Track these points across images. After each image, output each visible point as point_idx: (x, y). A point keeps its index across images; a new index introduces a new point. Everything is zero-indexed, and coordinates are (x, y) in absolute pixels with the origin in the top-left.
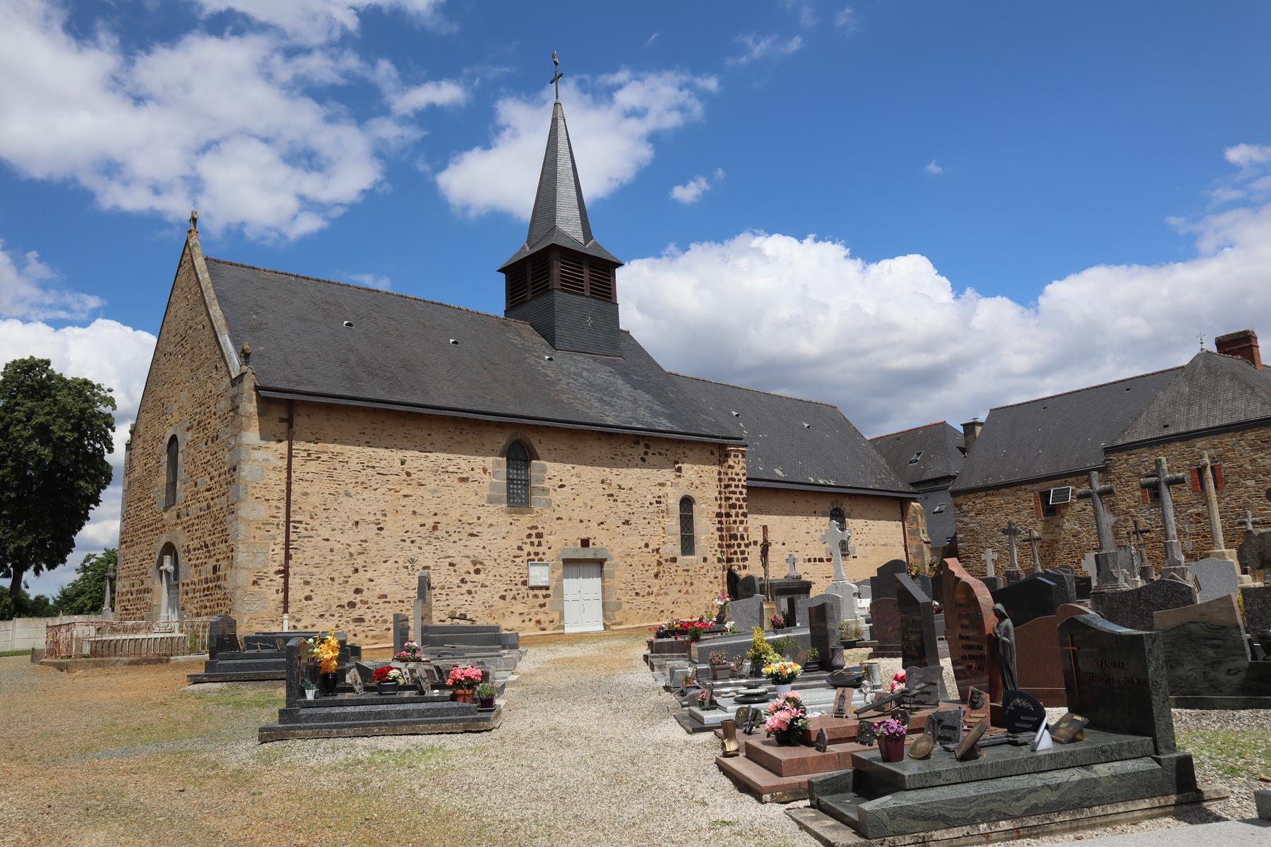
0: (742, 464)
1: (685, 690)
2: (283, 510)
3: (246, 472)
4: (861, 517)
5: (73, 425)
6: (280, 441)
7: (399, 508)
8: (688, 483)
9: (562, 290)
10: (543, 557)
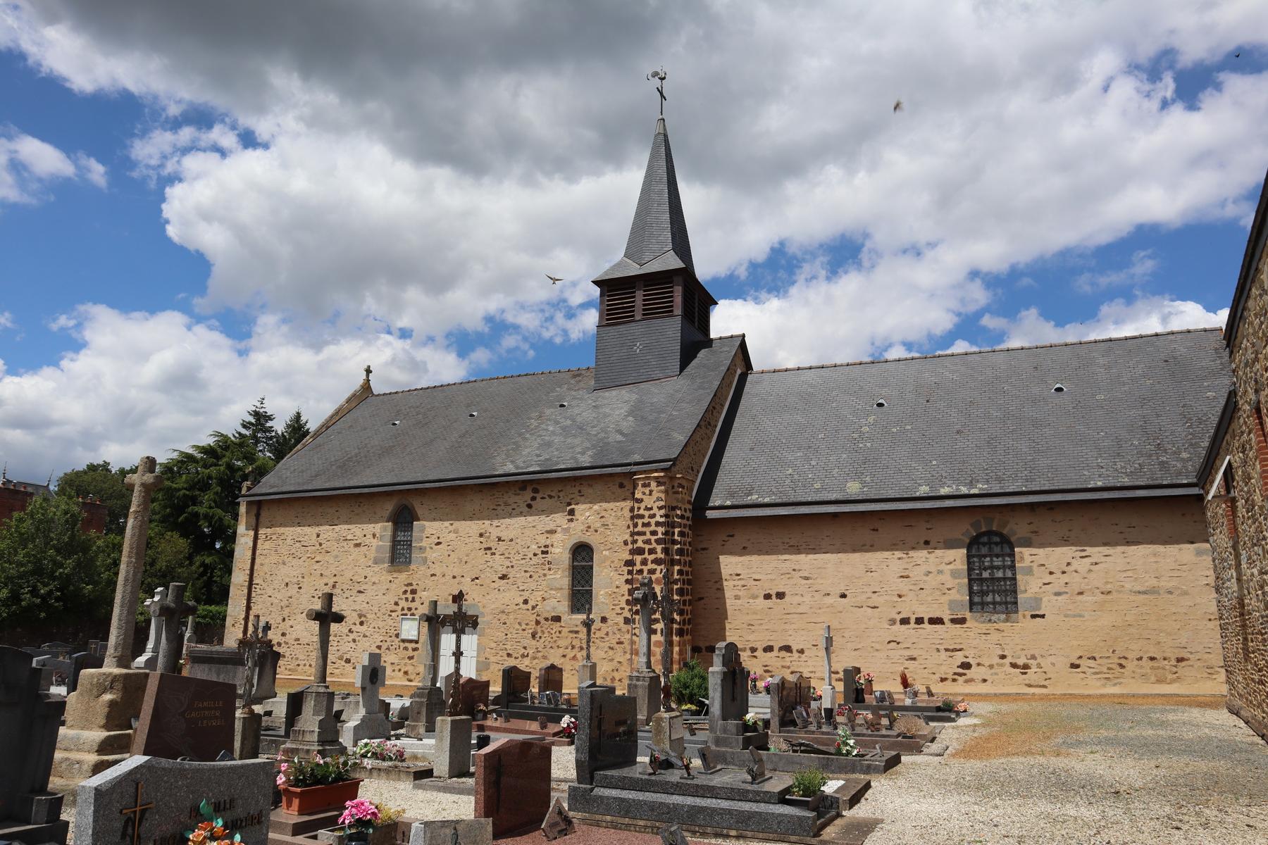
8: (583, 527)
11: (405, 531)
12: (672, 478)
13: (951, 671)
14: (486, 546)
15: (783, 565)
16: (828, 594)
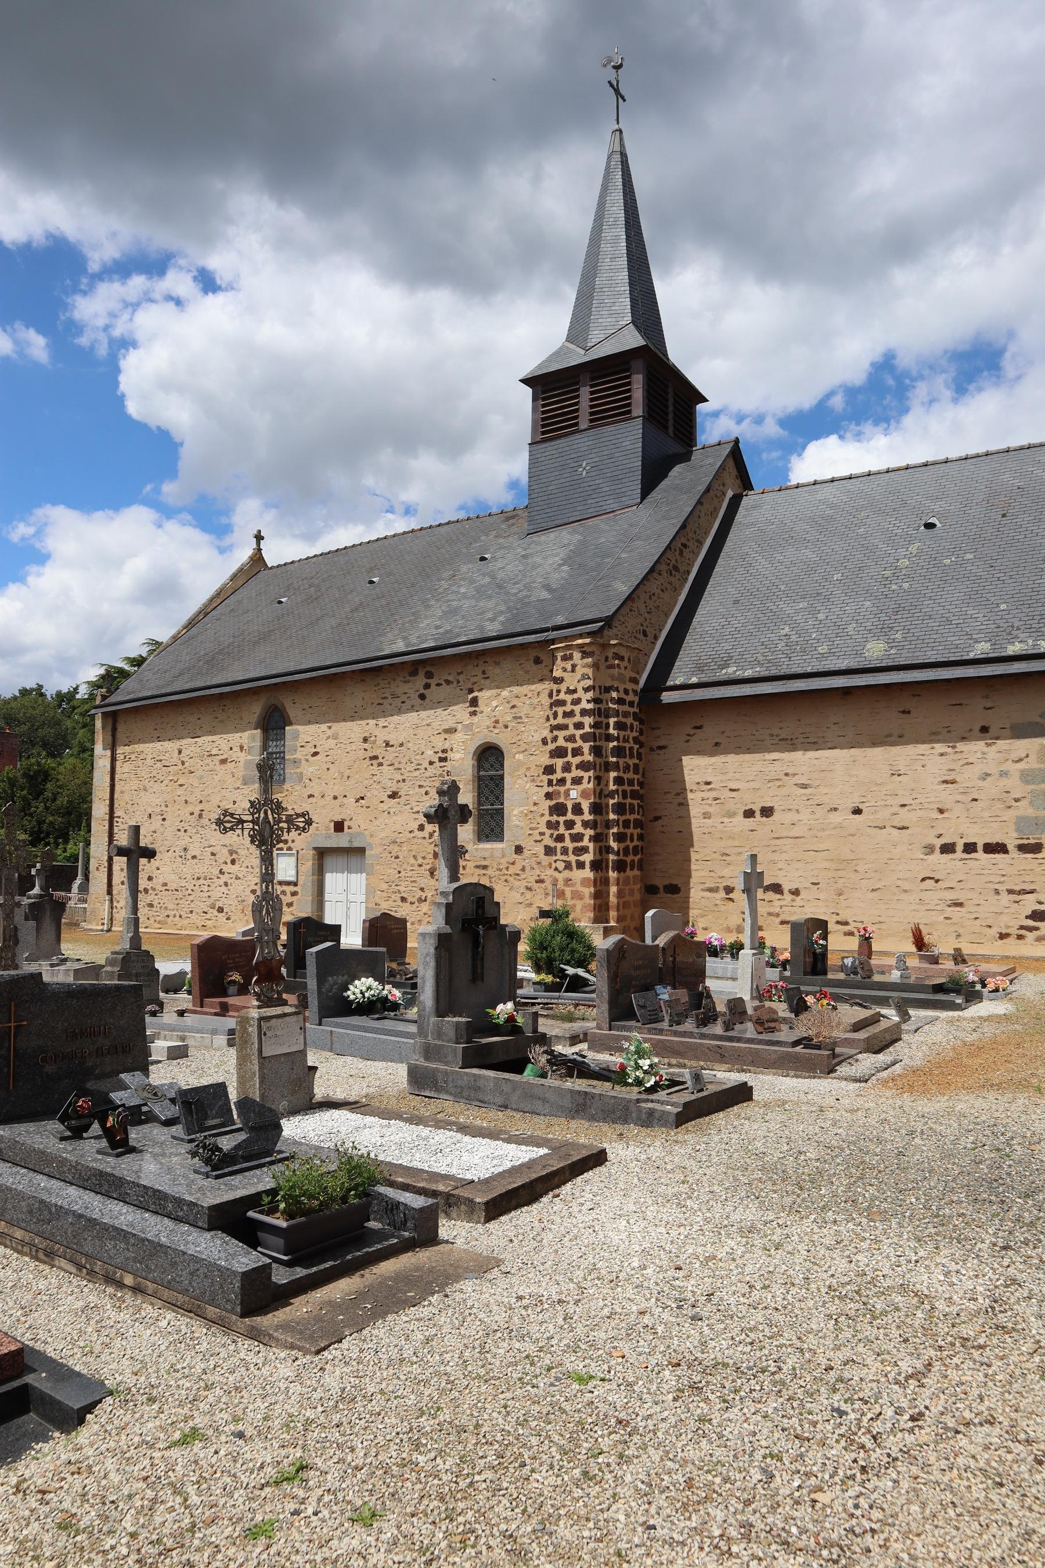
8: (489, 722)
11: (277, 740)
12: (605, 646)
13: (1016, 924)
14: (371, 755)
15: (771, 768)
16: (836, 809)
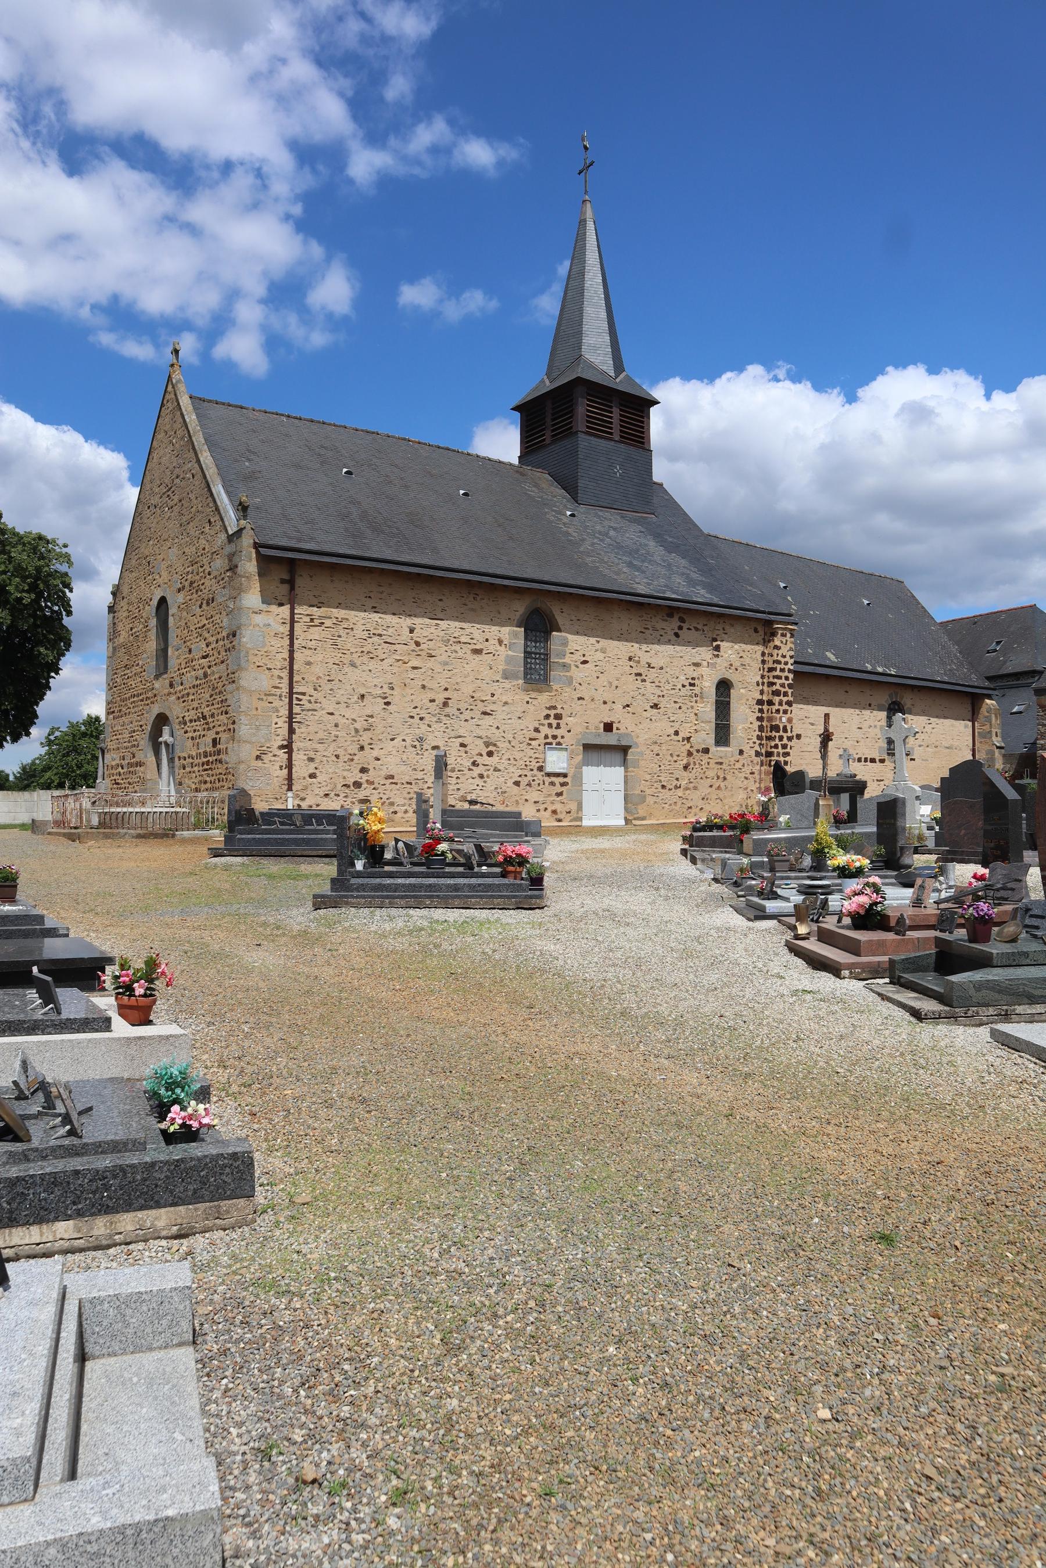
0: (790, 645)
1: (739, 881)
2: (286, 681)
3: (247, 638)
4: (923, 713)
5: (29, 584)
6: (281, 605)
7: (408, 681)
8: (726, 664)
9: (587, 433)
10: (562, 741)
